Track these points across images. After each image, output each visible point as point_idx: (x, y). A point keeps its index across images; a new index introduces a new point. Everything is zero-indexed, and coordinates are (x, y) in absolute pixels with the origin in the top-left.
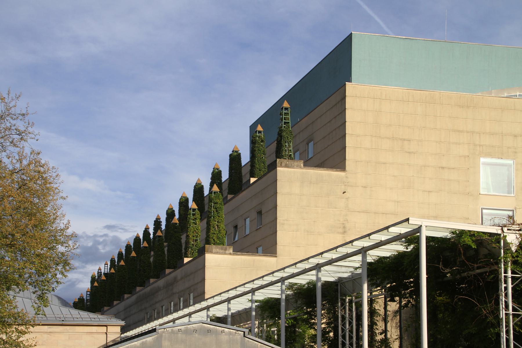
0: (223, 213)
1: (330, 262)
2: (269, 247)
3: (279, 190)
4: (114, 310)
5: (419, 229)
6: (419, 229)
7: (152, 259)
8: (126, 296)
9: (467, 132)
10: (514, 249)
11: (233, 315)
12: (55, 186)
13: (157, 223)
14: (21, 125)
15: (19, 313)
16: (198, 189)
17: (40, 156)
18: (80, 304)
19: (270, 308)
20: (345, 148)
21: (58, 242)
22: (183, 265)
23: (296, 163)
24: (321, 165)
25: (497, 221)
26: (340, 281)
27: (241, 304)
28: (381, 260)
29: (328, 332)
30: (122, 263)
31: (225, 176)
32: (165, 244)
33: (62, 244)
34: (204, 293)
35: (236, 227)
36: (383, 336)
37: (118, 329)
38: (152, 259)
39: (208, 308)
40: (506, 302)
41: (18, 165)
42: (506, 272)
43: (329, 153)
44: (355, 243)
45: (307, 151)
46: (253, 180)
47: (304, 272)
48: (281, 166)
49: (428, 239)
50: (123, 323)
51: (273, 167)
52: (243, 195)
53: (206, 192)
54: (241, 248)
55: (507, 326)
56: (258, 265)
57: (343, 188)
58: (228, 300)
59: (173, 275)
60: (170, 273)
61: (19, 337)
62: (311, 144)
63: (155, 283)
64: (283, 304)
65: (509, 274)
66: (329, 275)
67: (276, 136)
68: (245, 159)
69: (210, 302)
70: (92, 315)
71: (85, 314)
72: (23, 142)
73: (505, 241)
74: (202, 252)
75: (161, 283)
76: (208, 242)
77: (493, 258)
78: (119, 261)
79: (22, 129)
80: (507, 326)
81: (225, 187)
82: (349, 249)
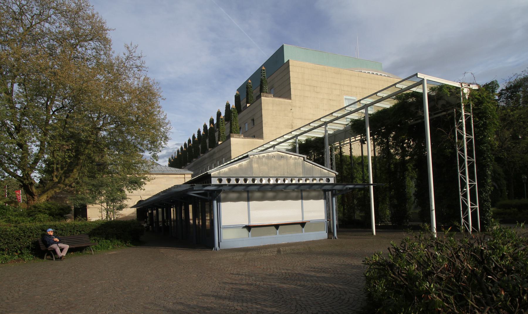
0: (238, 119)
1: (331, 121)
14: (138, 63)
21: (161, 126)
23: (270, 95)
31: (215, 122)
34: (231, 157)
37: (190, 176)
43: (284, 91)
46: (248, 105)
47: (357, 111)
50: (192, 173)
53: (208, 127)
54: (247, 135)
57: (291, 108)
59: (212, 151)
69: (232, 161)
75: (206, 155)
76: (231, 132)
79: (139, 64)
81: (215, 126)
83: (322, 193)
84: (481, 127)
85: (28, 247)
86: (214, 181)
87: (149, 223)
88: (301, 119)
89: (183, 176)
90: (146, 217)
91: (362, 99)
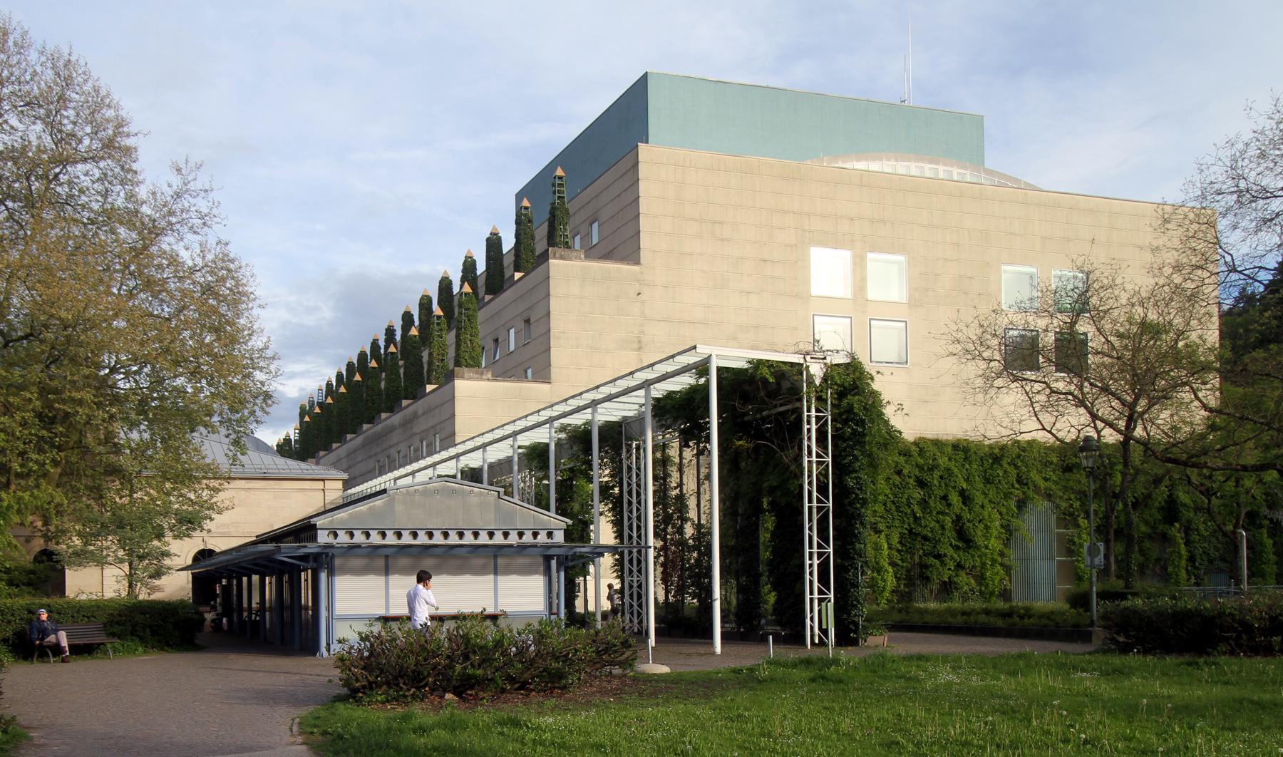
1: (609, 398)
2: (542, 373)
3: (640, 176)
4: (332, 457)
5: (707, 360)
6: (707, 360)
7: (383, 385)
8: (349, 436)
9: (794, 213)
10: (818, 382)
11: (491, 466)
12: (251, 290)
14: (203, 206)
15: (208, 465)
16: (445, 285)
17: (229, 247)
18: (285, 449)
19: (537, 455)
22: (425, 395)
24: (607, 256)
25: (802, 346)
28: (670, 394)
29: (612, 488)
30: (342, 390)
32: (401, 363)
33: (261, 369)
34: (454, 434)
35: (496, 340)
36: (677, 491)
37: (340, 485)
38: (383, 385)
39: (457, 456)
40: (809, 447)
41: (199, 262)
42: (809, 411)
44: (636, 375)
45: (589, 234)
46: (517, 276)
47: (579, 410)
48: (554, 257)
49: (719, 369)
51: (544, 257)
53: (456, 290)
55: (810, 476)
56: (531, 395)
58: (484, 446)
59: (411, 409)
60: (408, 406)
61: (212, 497)
62: (595, 226)
63: (388, 420)
65: (813, 413)
66: (610, 413)
67: (547, 216)
68: (508, 243)
69: (460, 449)
70: (303, 465)
71: (294, 466)
72: (206, 229)
73: (808, 372)
74: (450, 377)
75: (396, 419)
77: (795, 394)
78: (338, 385)
79: (205, 210)
80: (810, 476)
81: (481, 282)
82: (630, 382)
83: (541, 560)
84: (849, 439)
86: (323, 538)
89: (320, 485)
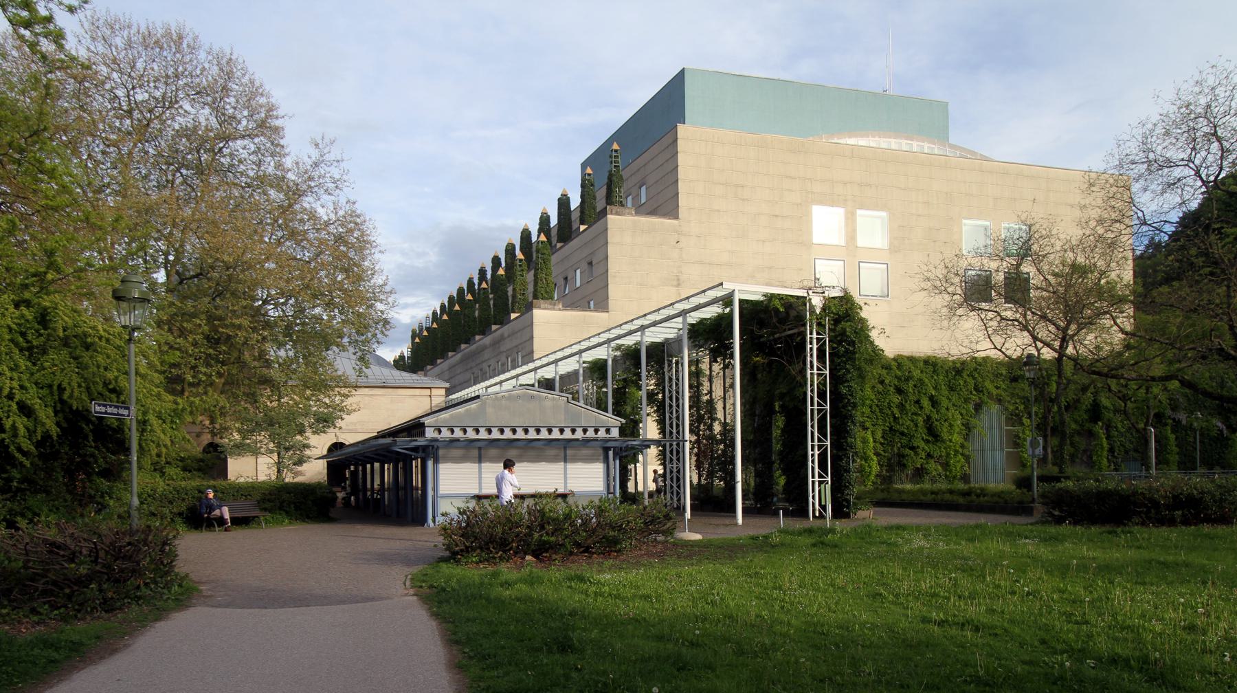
1: (654, 324)
4: (437, 370)
5: (731, 294)
6: (731, 294)
7: (477, 314)
8: (450, 354)
10: (818, 311)
11: (561, 377)
13: (482, 272)
16: (526, 235)
18: (400, 364)
19: (597, 369)
20: (677, 194)
22: (510, 321)
24: (653, 212)
25: (805, 283)
26: (667, 342)
27: (566, 367)
28: (702, 321)
30: (445, 317)
33: (381, 301)
34: (532, 352)
35: (566, 279)
37: (443, 392)
38: (477, 314)
39: (535, 370)
41: (333, 217)
43: (664, 203)
46: (582, 228)
51: (603, 213)
52: (574, 244)
53: (534, 239)
58: (556, 362)
59: (499, 332)
62: (644, 188)
64: (610, 362)
65: (815, 336)
66: (655, 336)
67: (606, 181)
68: (575, 202)
69: (538, 363)
70: (414, 376)
71: (407, 377)
74: (529, 307)
75: (487, 340)
76: (535, 297)
77: (800, 321)
78: (442, 313)
79: (337, 177)
81: (554, 233)
83: (601, 451)
85: (180, 514)
86: (430, 433)
87: (349, 489)
88: (701, 263)
89: (427, 392)
90: (345, 479)
91: (664, 308)
